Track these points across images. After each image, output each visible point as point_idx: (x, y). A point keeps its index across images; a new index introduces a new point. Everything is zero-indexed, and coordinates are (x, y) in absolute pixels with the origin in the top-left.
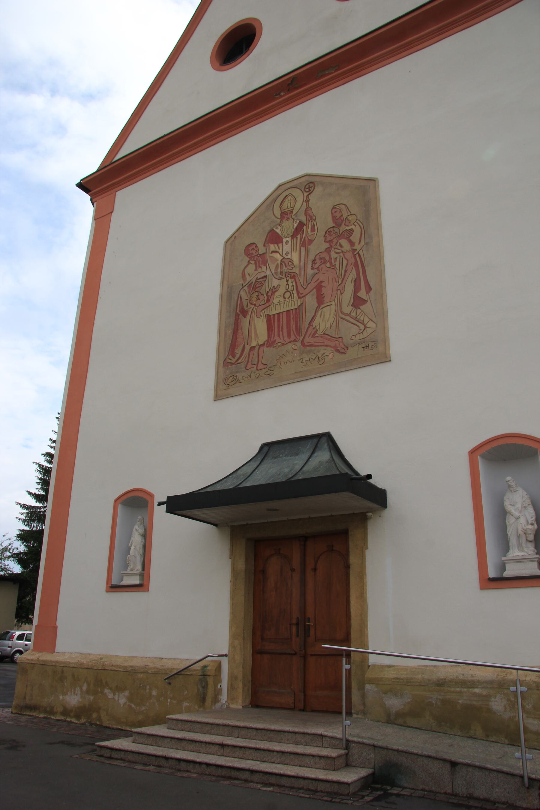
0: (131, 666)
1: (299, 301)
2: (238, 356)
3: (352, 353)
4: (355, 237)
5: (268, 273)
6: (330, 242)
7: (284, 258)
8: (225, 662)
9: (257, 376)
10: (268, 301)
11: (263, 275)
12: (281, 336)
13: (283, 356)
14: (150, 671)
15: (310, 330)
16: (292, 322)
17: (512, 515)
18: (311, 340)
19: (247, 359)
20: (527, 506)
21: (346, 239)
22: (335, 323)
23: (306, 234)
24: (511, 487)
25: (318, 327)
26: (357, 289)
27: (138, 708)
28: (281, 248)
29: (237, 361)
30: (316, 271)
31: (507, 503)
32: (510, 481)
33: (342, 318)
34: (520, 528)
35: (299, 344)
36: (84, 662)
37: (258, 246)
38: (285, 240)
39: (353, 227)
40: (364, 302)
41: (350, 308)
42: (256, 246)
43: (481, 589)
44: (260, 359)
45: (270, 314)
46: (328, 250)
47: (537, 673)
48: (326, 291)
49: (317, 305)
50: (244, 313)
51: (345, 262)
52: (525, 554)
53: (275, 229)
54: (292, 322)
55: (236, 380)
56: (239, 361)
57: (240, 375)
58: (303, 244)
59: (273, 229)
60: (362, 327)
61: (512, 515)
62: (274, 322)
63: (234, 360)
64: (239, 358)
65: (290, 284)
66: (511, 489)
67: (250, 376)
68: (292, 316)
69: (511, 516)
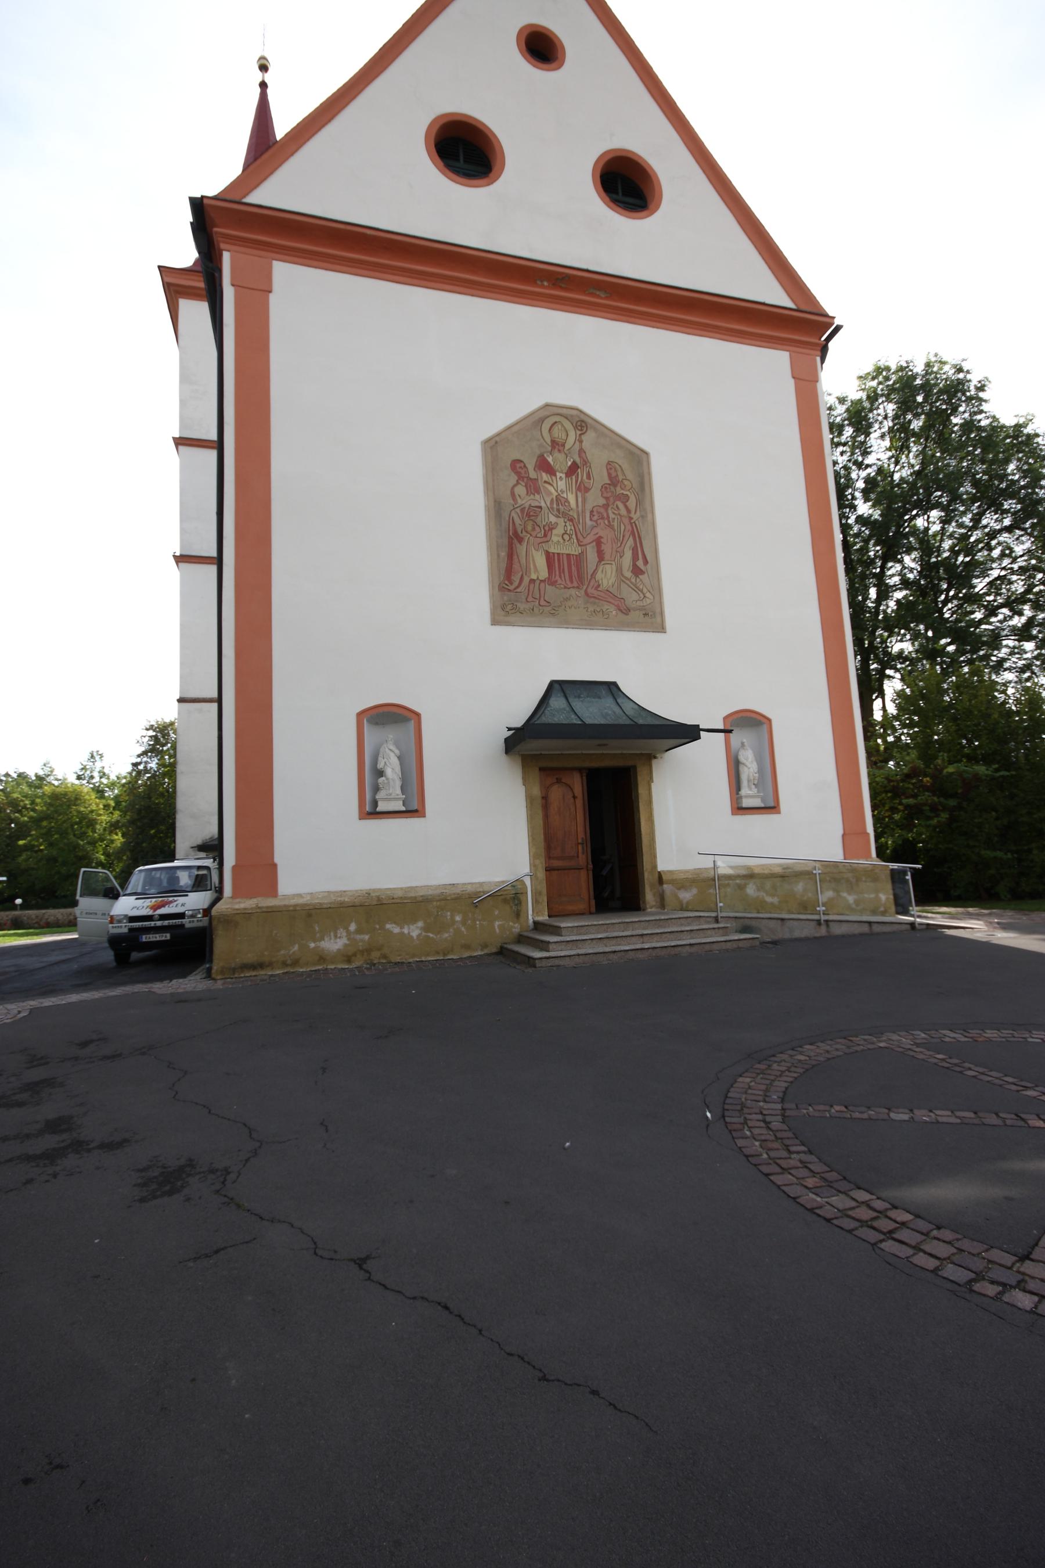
0: (422, 896)
1: (580, 548)
2: (516, 584)
3: (634, 615)
4: (632, 503)
5: (543, 504)
6: (607, 499)
7: (559, 495)
8: (528, 881)
9: (541, 611)
10: (545, 535)
11: (537, 504)
12: (563, 579)
13: (567, 599)
14: (449, 898)
15: (593, 581)
16: (574, 568)
18: (596, 593)
19: (527, 590)
21: (622, 502)
22: (616, 584)
23: (582, 479)
25: (600, 582)
26: (635, 558)
27: (438, 936)
28: (555, 481)
29: (515, 589)
30: (594, 524)
33: (623, 581)
35: (583, 592)
36: (346, 900)
37: (527, 465)
38: (558, 475)
39: (628, 493)
40: (642, 572)
41: (630, 574)
42: (525, 466)
43: (732, 814)
44: (542, 595)
45: (550, 551)
46: (606, 507)
48: (607, 548)
49: (597, 560)
50: (520, 540)
51: (623, 527)
53: (545, 455)
54: (574, 568)
55: (515, 610)
56: (518, 590)
57: (522, 606)
58: (579, 489)
59: (543, 455)
60: (642, 595)
62: (554, 560)
63: (511, 587)
64: (517, 587)
65: (569, 528)
67: (533, 610)
68: (572, 563)
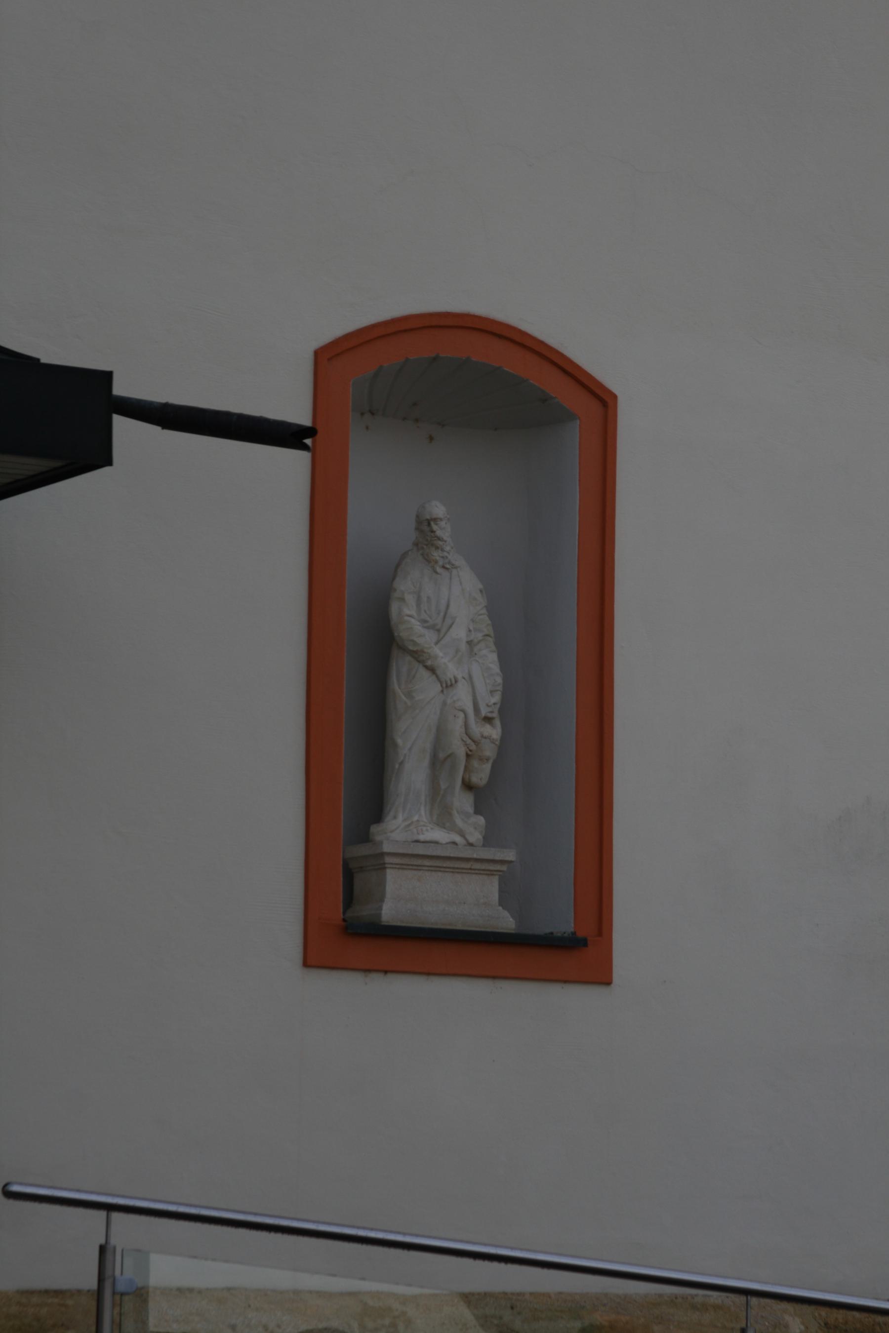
17: (432, 670)
20: (479, 642)
24: (437, 548)
31: (408, 612)
32: (441, 520)
34: (457, 726)
43: (307, 964)
47: (824, 1312)
52: (458, 839)
61: (432, 670)
66: (436, 555)
69: (423, 673)
